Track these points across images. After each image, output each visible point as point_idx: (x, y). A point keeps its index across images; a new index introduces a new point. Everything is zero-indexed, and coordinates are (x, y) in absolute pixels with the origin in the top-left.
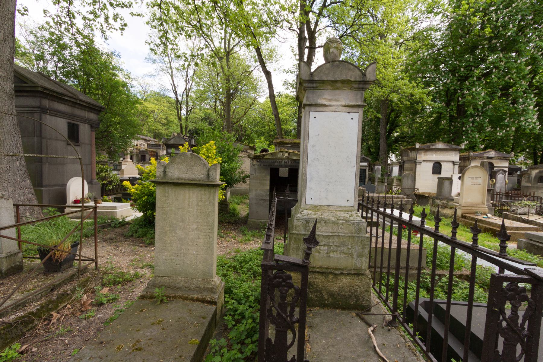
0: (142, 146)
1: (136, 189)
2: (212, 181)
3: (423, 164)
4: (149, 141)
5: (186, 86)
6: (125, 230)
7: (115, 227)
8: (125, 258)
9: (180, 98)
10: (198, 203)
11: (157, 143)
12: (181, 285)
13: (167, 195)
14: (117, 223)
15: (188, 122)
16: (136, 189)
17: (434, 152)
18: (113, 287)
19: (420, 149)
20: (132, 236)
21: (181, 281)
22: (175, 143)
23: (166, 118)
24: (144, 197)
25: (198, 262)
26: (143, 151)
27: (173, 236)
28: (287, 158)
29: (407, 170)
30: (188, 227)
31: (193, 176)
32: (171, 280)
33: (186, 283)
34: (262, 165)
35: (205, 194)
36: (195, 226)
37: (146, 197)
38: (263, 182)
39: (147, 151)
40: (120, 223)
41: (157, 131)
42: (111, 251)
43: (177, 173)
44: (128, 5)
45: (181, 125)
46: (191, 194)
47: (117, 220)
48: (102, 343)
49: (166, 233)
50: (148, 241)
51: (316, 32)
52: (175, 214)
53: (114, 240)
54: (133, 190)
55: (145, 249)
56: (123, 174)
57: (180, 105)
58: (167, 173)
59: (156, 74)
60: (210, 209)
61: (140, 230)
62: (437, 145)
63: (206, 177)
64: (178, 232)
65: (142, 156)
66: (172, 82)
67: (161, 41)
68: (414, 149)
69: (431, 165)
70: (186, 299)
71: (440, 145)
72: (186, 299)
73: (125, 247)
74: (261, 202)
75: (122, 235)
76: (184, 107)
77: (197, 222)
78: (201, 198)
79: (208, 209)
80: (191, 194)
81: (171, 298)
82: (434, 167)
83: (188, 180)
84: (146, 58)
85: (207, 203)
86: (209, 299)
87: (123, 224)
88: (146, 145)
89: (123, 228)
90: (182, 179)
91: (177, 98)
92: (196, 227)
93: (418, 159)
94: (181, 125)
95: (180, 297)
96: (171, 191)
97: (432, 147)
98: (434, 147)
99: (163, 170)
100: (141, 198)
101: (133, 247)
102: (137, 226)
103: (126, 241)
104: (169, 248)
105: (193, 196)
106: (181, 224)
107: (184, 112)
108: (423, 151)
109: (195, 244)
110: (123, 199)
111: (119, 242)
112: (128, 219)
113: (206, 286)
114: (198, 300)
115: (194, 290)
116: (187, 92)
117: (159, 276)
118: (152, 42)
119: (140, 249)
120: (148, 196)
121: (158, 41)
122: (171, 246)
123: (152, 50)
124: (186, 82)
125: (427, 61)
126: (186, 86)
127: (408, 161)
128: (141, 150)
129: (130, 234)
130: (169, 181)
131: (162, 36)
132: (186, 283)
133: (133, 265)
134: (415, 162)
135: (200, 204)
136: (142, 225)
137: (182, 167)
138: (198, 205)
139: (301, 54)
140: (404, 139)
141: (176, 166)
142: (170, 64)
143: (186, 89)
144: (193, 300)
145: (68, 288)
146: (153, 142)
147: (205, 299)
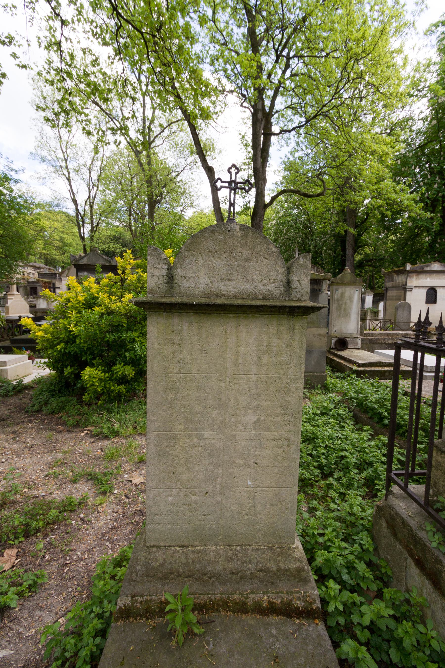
0: (31, 276)
1: (46, 332)
2: (299, 300)
3: (415, 290)
4: (39, 268)
5: (90, 192)
6: (26, 400)
7: (7, 396)
8: (35, 459)
10: (260, 358)
11: (52, 271)
12: (219, 567)
13: (176, 339)
14: (10, 388)
16: (46, 332)
17: (428, 275)
18: (26, 546)
20: (40, 411)
21: (216, 555)
22: (89, 263)
23: (61, 240)
24: (58, 344)
25: (259, 507)
26: (33, 282)
27: (193, 446)
29: (391, 299)
30: (233, 420)
31: (246, 287)
32: (191, 556)
33: (230, 560)
35: (279, 335)
36: (251, 418)
37: (62, 344)
39: (38, 281)
40: (14, 388)
41: (49, 257)
42: (5, 444)
43: (205, 280)
44: (7, 41)
45: (84, 246)
46: (243, 335)
47: (8, 382)
49: (175, 438)
50: (71, 422)
52: (198, 389)
53: (9, 422)
54: (40, 334)
55: (67, 435)
56: (7, 313)
58: (177, 279)
59: (46, 176)
60: (291, 371)
61: (54, 402)
62: (433, 266)
63: (282, 289)
64: (206, 435)
65: (31, 288)
66: (69, 188)
67: (61, 107)
68: (404, 272)
71: (436, 266)
73: (32, 435)
75: (22, 409)
76: (87, 220)
77: (257, 407)
78: (269, 345)
79: (286, 373)
80: (243, 335)
82: (428, 294)
83: (235, 297)
84: (31, 153)
85: (284, 358)
86: (300, 604)
87: (20, 389)
88: (37, 275)
89: (21, 396)
90: (219, 296)
91: (77, 210)
92: (254, 419)
93: (409, 284)
96: (188, 329)
97: (426, 269)
98: (428, 269)
99: (165, 272)
100: (53, 346)
101: (47, 434)
102: (47, 393)
103: (30, 421)
104: (185, 476)
105: (248, 340)
106: (214, 413)
107: (88, 227)
108: (414, 274)
109: (251, 462)
110: (15, 349)
111: (18, 424)
112: (27, 380)
114: (272, 610)
115: (253, 577)
116: (90, 201)
117: (158, 547)
118: (47, 107)
120: (67, 343)
121: (56, 107)
122: (189, 470)
123: (47, 120)
124: (89, 188)
125: (409, 160)
126: (90, 192)
127: (393, 287)
128: (30, 280)
129: (35, 408)
130: (185, 300)
131: (63, 99)
132: (230, 560)
133: (56, 476)
134: (404, 288)
135: (265, 360)
136: (54, 391)
137: (219, 263)
138: (259, 364)
141: (201, 261)
142: (66, 162)
143: (89, 197)
144: (258, 609)
146: (46, 270)
147: (289, 603)
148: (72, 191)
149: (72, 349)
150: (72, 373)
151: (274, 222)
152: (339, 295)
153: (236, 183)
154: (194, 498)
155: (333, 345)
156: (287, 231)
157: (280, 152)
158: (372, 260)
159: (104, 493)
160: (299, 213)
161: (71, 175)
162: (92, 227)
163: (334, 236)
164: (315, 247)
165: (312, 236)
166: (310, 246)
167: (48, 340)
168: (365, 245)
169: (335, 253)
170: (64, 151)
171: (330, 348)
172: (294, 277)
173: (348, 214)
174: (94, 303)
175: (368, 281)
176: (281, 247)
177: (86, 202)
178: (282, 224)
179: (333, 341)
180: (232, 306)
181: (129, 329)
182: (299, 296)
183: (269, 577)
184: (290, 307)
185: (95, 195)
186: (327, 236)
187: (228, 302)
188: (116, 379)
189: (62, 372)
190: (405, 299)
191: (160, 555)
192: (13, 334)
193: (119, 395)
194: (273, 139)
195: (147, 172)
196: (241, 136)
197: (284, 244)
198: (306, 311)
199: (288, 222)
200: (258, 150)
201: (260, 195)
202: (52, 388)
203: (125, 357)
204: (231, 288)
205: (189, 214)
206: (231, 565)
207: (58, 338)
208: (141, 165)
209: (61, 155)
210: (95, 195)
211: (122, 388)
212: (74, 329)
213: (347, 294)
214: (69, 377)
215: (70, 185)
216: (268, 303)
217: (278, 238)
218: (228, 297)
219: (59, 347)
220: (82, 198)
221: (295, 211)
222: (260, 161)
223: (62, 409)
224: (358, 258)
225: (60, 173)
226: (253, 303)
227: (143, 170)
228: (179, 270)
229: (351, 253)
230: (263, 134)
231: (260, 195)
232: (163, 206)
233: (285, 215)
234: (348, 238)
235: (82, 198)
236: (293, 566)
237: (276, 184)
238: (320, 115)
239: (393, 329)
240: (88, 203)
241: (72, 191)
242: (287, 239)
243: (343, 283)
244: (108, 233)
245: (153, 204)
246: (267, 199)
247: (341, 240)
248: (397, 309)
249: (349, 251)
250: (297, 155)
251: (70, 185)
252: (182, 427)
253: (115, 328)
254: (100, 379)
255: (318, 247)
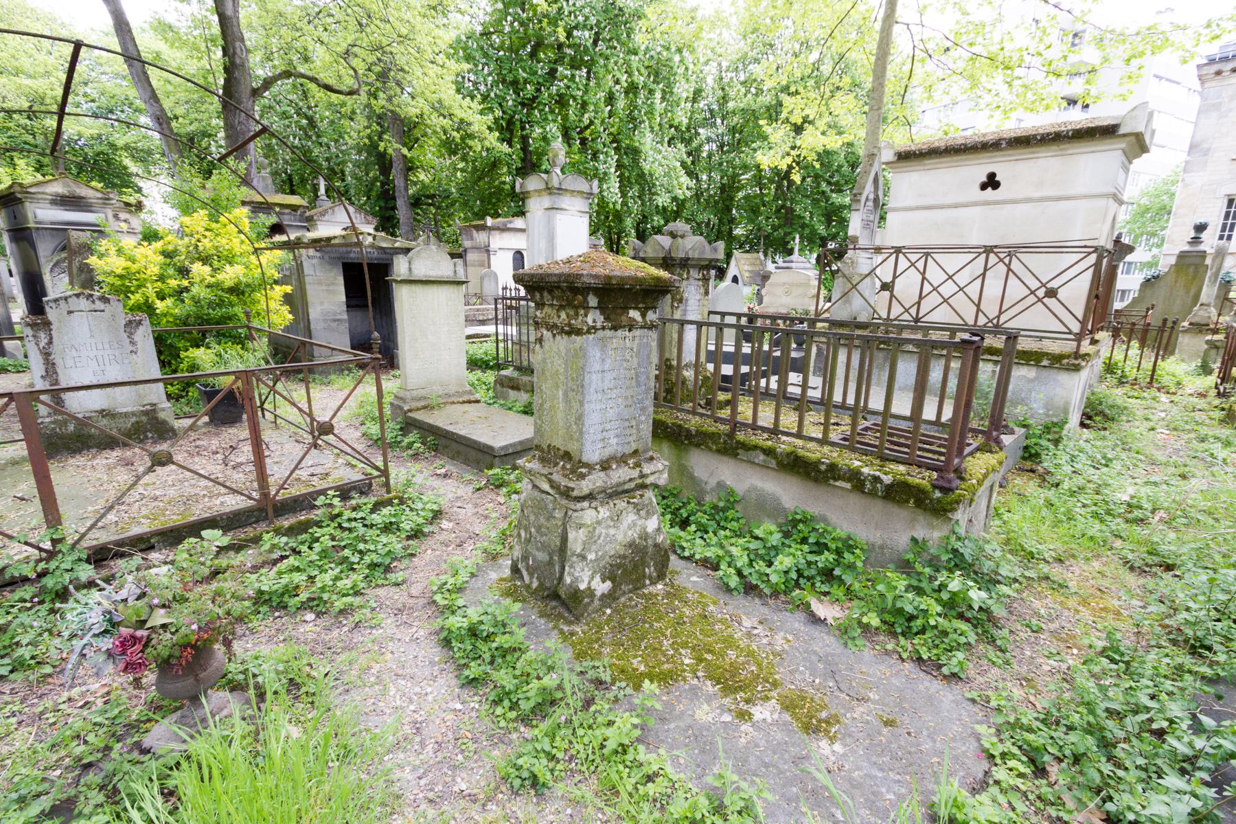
3: (500, 253)
19: (491, 229)
28: (372, 246)
29: (473, 265)
34: (326, 257)
38: (331, 288)
68: (483, 228)
69: (510, 255)
74: (334, 325)
96: (418, 289)
97: (509, 226)
108: (497, 232)
114: (464, 402)
183: (458, 394)
190: (489, 267)
198: (463, 283)
229: (402, 184)
239: (481, 304)
248: (482, 279)
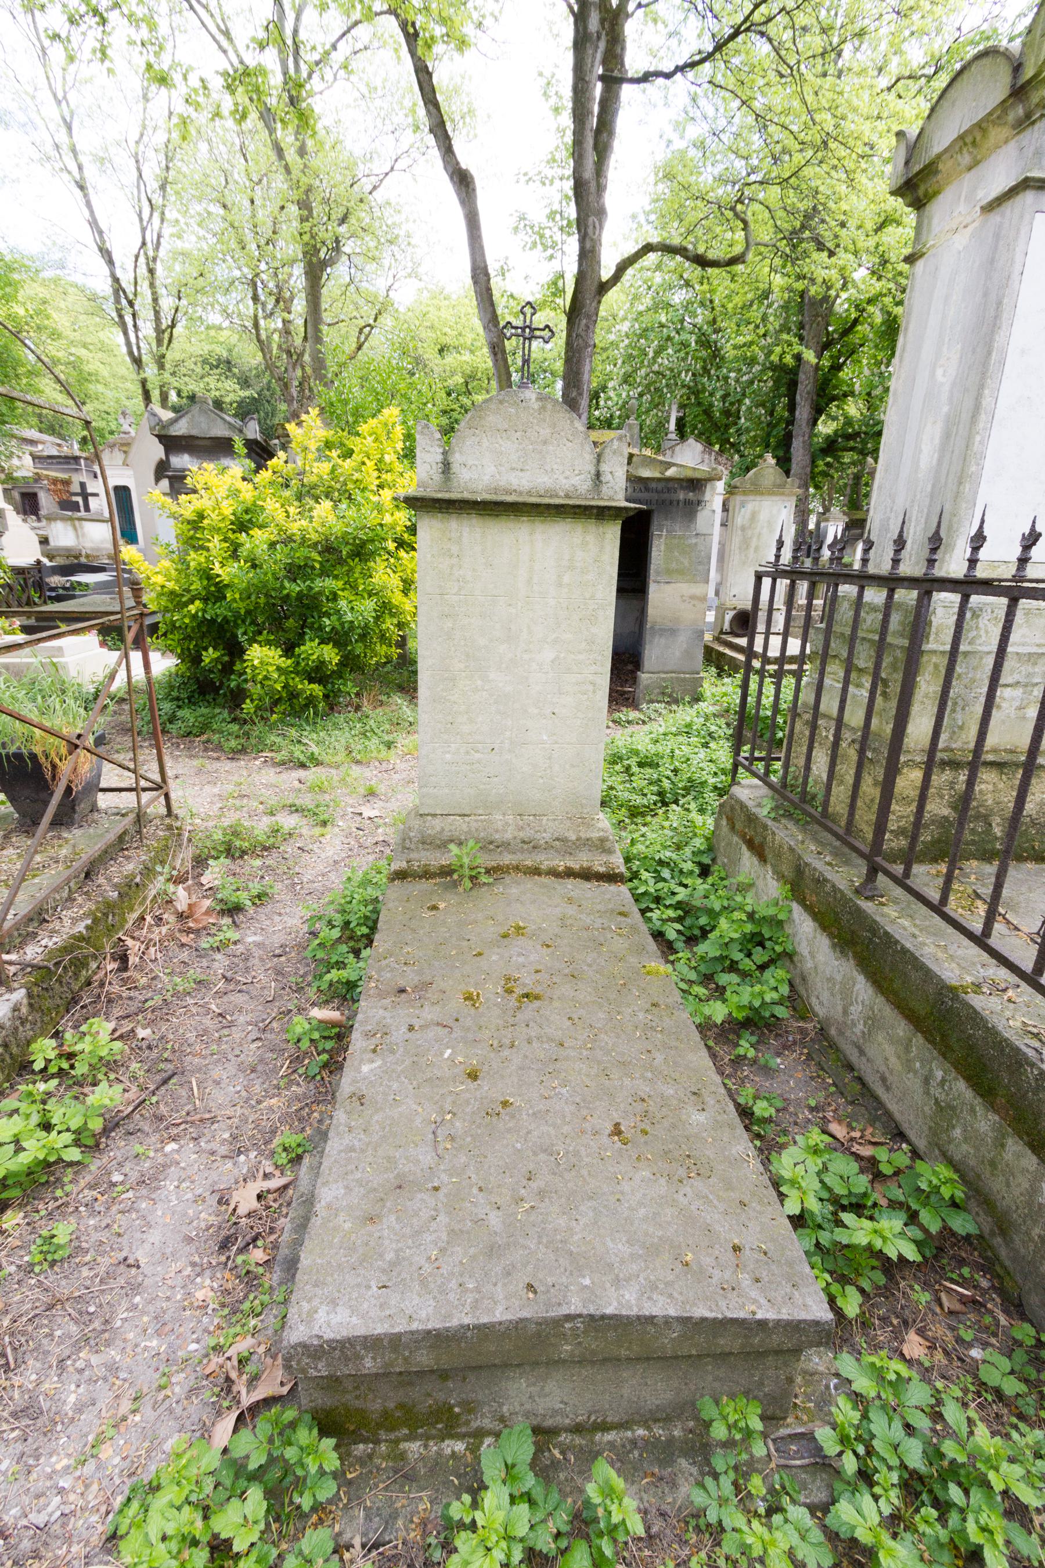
2: (611, 499)
5: (143, 230)
9: (126, 280)
12: (508, 836)
13: (455, 549)
15: (167, 375)
21: (505, 826)
22: (194, 432)
30: (526, 656)
32: (474, 825)
36: (548, 654)
37: (197, 603)
43: (491, 469)
45: (144, 383)
48: (402, 991)
51: (628, 16)
55: (229, 765)
57: (131, 304)
58: (455, 468)
63: (589, 483)
65: (24, 495)
70: (536, 871)
72: (536, 871)
81: (496, 871)
83: (529, 493)
86: (602, 870)
91: (116, 280)
94: (144, 383)
95: (517, 868)
96: (469, 532)
99: (439, 458)
107: (147, 329)
113: (583, 835)
114: (570, 873)
115: (548, 847)
119: (217, 765)
120: (205, 600)
124: (141, 220)
130: (466, 496)
135: (566, 579)
138: (560, 585)
139: (580, 113)
140: (852, 443)
141: (485, 443)
143: (144, 244)
144: (554, 873)
145: (129, 866)
148: (94, 223)
149: (217, 611)
150: (217, 660)
151: (625, 327)
152: (748, 516)
153: (532, 330)
154: (478, 756)
155: (727, 626)
156: (658, 353)
157: (646, 127)
158: (857, 434)
159: (324, 823)
160: (690, 303)
161: (86, 173)
162: (159, 331)
163: (774, 368)
164: (724, 398)
165: (719, 367)
166: (711, 394)
167: (172, 593)
168: (845, 395)
169: (771, 414)
170: (60, 96)
171: (722, 632)
172: (604, 468)
173: (809, 312)
174: (250, 521)
175: (848, 491)
176: (641, 395)
177: (137, 257)
178: (645, 332)
179: (729, 617)
180: (525, 504)
181: (325, 573)
182: (611, 493)
184: (598, 507)
185: (159, 236)
186: (757, 368)
187: (520, 499)
188: (305, 671)
189: (197, 660)
191: (437, 824)
192: (29, 602)
193: (311, 701)
194: (627, 91)
195: (296, 173)
196: (543, 81)
197: (648, 386)
199: (662, 326)
200: (588, 126)
201: (588, 255)
202: (175, 694)
203: (321, 628)
204: (524, 482)
205: (405, 296)
206: (521, 834)
207: (188, 591)
208: (280, 152)
209: (51, 111)
210: (159, 236)
211: (317, 689)
212: (220, 572)
213: (763, 517)
214: (211, 671)
215: (89, 204)
216: (571, 502)
217: (635, 371)
218: (521, 493)
219: (193, 608)
220: (124, 244)
221: (679, 297)
222: (591, 157)
223: (205, 727)
224: (826, 428)
225: (58, 165)
226: (552, 501)
227: (287, 169)
228: (457, 455)
230: (602, 78)
231: (588, 255)
232: (338, 275)
233: (655, 308)
234: (802, 376)
235: (124, 244)
236: (595, 835)
237: (634, 217)
238: (747, 30)
240: (142, 260)
241: (94, 223)
242: (658, 373)
243: (757, 490)
244: (201, 348)
245: (315, 271)
246: (606, 273)
247: (787, 378)
249: (803, 412)
250: (694, 132)
251: (89, 204)
252: (462, 666)
253: (296, 571)
254: (278, 669)
255: (730, 399)
